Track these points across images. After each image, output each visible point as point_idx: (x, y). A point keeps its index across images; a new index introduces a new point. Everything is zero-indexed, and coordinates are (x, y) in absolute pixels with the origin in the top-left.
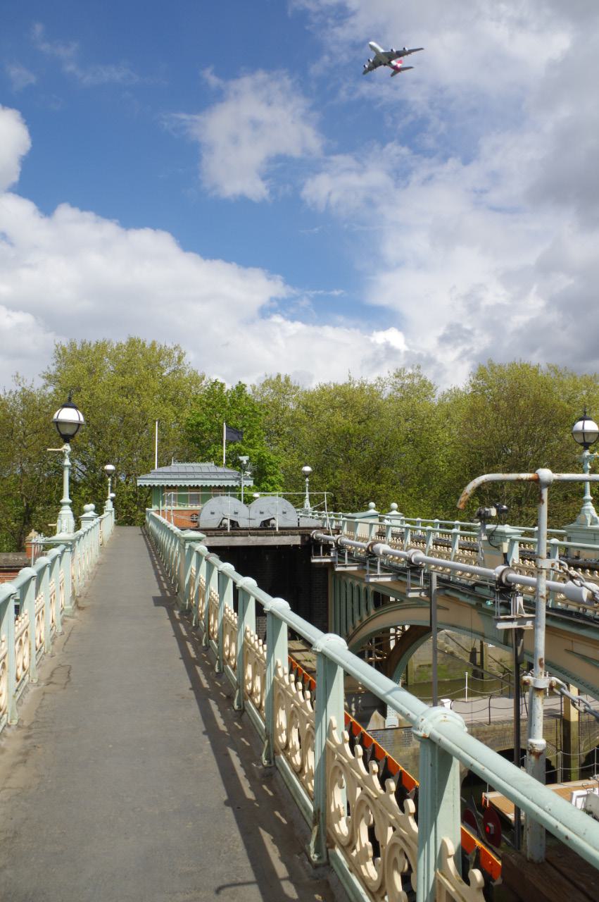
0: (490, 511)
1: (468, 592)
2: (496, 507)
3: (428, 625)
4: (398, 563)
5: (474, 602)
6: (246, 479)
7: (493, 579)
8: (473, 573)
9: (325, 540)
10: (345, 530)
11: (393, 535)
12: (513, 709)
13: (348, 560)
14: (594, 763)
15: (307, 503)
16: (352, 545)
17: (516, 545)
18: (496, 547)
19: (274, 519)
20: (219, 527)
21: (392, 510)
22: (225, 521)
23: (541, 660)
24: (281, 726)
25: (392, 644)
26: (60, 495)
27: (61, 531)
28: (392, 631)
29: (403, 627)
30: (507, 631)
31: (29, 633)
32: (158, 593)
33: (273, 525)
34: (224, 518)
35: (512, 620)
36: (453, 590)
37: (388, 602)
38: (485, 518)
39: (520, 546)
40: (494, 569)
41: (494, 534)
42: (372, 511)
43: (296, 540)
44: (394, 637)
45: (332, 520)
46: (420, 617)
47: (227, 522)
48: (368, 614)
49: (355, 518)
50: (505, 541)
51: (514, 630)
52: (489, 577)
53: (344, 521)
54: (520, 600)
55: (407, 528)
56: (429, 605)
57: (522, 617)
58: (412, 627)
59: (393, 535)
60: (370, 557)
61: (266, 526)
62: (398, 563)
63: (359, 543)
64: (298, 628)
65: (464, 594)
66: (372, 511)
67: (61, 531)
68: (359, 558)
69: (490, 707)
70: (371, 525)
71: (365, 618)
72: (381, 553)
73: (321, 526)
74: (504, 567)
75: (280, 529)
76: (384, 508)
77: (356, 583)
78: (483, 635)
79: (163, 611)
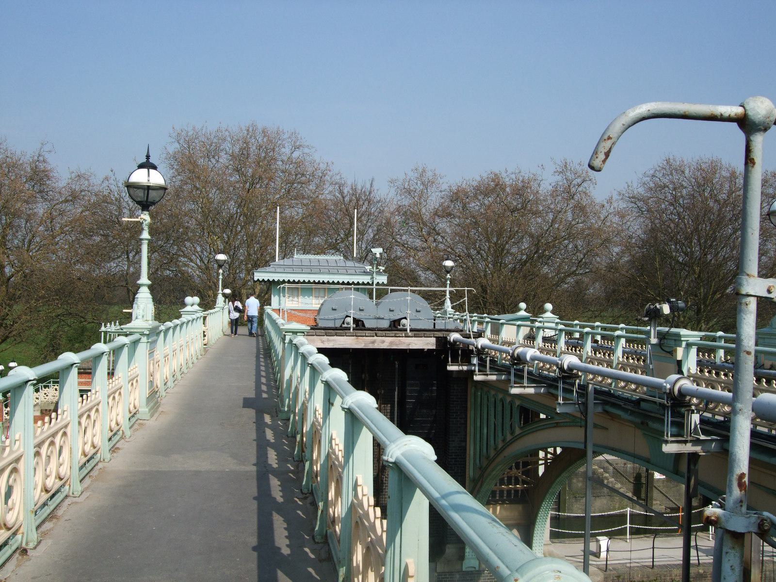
0: (662, 308)
1: (630, 408)
2: (669, 302)
3: (582, 446)
4: (549, 372)
5: (638, 420)
6: (379, 273)
7: (664, 391)
8: (638, 383)
9: (464, 344)
10: (488, 332)
11: (545, 339)
12: (682, 549)
13: (490, 368)
14: (626, 524)
15: (448, 304)
16: (496, 350)
17: (694, 350)
18: (669, 352)
19: (405, 318)
20: (341, 326)
21: (545, 312)
22: (348, 319)
23: (742, 476)
24: (358, 566)
25: (541, 470)
26: (138, 275)
27: (137, 318)
28: (542, 454)
29: (555, 450)
30: (678, 456)
31: (100, 410)
32: (252, 395)
33: (404, 325)
34: (347, 316)
35: (685, 442)
36: (614, 405)
37: (536, 419)
38: (655, 316)
39: (698, 355)
40: (664, 378)
41: (666, 337)
42: (522, 313)
43: (428, 343)
44: (543, 462)
45: (472, 322)
46: (573, 436)
47: (350, 320)
48: (512, 433)
49: (499, 320)
50: (680, 346)
51: (687, 455)
52: (659, 387)
53: (487, 322)
54: (695, 418)
55: (561, 330)
56: (583, 423)
57: (698, 439)
58: (564, 449)
59: (545, 339)
60: (515, 364)
61: (395, 326)
62: (549, 372)
63: (505, 347)
64: (363, 416)
65: (626, 410)
66: (522, 313)
67: (137, 318)
68: (504, 366)
69: (653, 548)
70: (519, 326)
71: (509, 437)
72: (528, 358)
73: (461, 328)
74: (678, 376)
75: (411, 330)
76: (536, 310)
77: (500, 396)
78: (648, 461)
79: (251, 413)
